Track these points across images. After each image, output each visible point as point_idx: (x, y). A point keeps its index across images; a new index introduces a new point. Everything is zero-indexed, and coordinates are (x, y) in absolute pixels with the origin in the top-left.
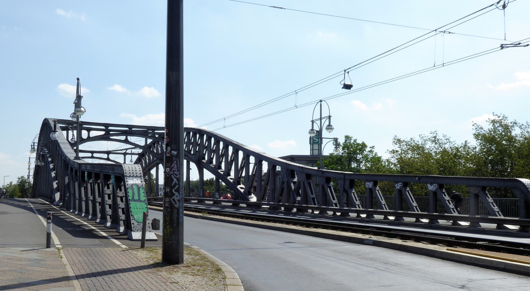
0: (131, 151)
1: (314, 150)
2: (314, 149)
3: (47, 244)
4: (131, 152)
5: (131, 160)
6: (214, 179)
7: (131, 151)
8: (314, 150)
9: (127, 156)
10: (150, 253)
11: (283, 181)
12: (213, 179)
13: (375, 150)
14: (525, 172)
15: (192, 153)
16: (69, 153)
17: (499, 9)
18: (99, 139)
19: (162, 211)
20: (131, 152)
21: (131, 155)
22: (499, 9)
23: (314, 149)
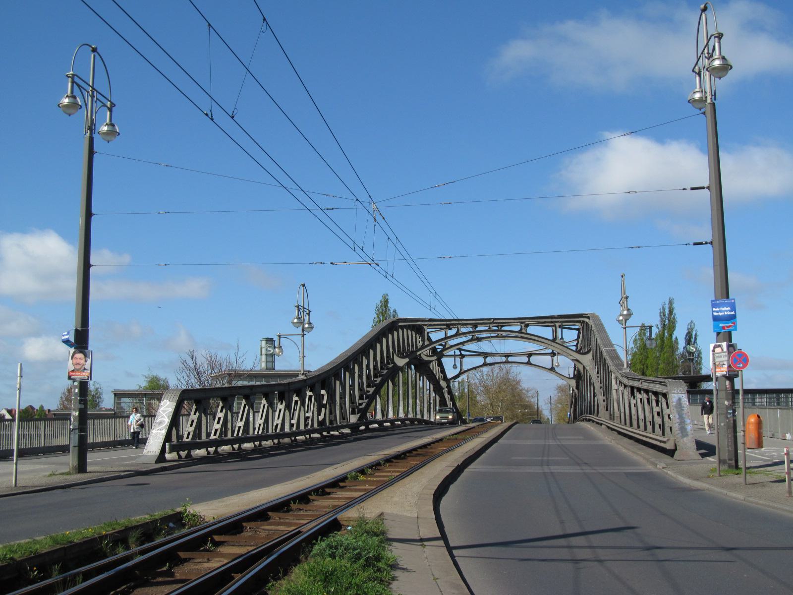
0: (455, 352)
5: (455, 365)
7: (455, 352)
9: (465, 360)
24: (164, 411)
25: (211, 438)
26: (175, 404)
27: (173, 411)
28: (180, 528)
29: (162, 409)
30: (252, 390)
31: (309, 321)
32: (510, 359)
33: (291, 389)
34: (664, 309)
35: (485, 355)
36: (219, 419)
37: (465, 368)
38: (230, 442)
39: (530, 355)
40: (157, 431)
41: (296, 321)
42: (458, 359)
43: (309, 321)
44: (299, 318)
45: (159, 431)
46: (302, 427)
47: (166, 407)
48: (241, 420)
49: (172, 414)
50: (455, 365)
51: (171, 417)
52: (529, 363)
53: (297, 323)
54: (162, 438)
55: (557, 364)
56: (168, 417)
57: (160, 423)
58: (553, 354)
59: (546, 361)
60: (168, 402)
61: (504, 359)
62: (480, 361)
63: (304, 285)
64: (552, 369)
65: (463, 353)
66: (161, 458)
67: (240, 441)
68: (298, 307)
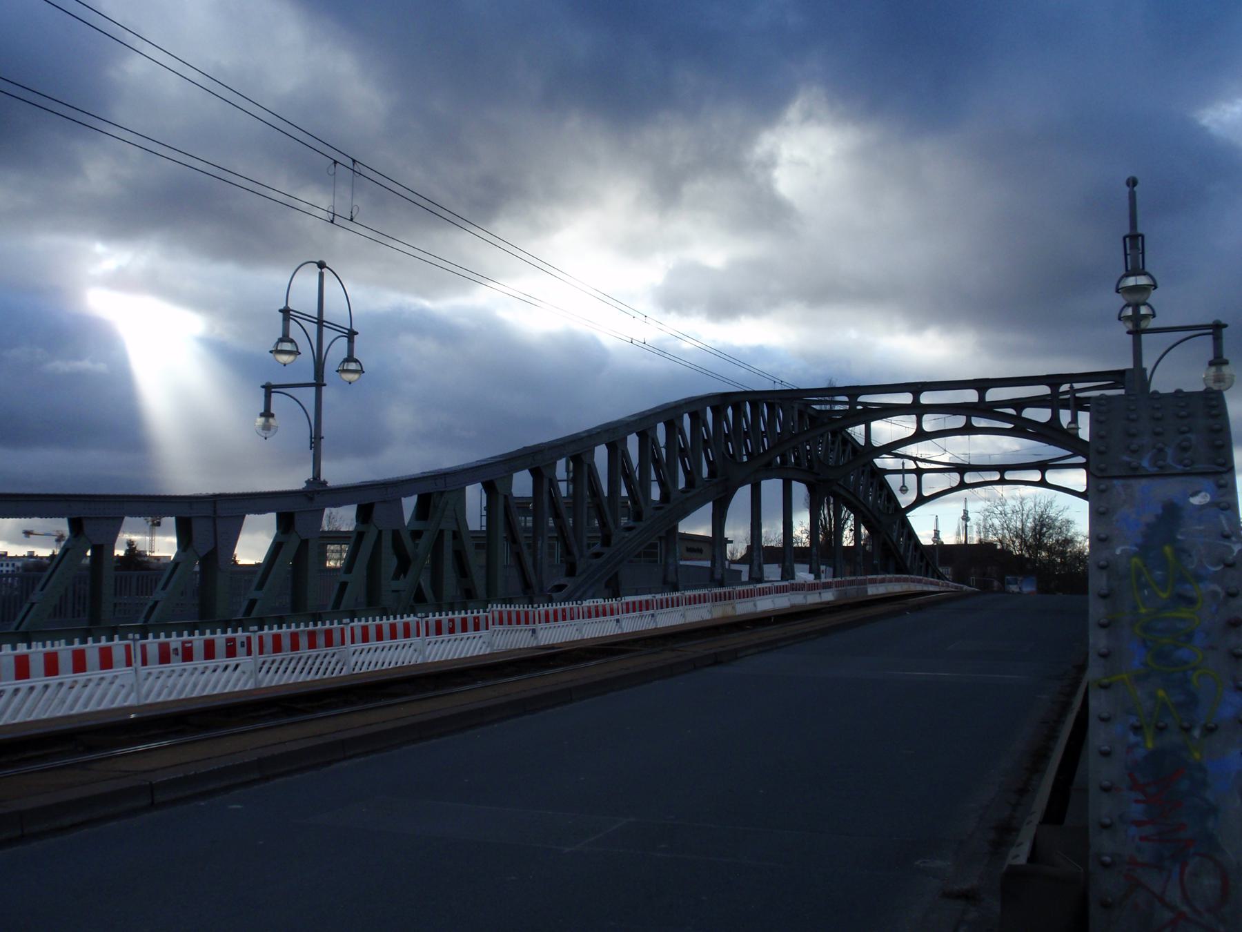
1: (903, 477)
2: (313, 389)
3: (281, 547)
4: (903, 467)
5: (904, 486)
6: (172, 558)
8: (903, 477)
9: (925, 476)
10: (156, 561)
11: (441, 527)
12: (170, 557)
13: (145, 522)
14: (1189, 435)
15: (745, 459)
16: (852, 473)
17: (458, 524)
18: (148, 569)
19: (759, 485)
20: (903, 467)
21: (901, 475)
22: (458, 524)
23: (313, 389)
35: (961, 469)
37: (926, 493)
39: (1043, 466)
42: (913, 477)
52: (1043, 483)
62: (955, 478)
65: (922, 465)
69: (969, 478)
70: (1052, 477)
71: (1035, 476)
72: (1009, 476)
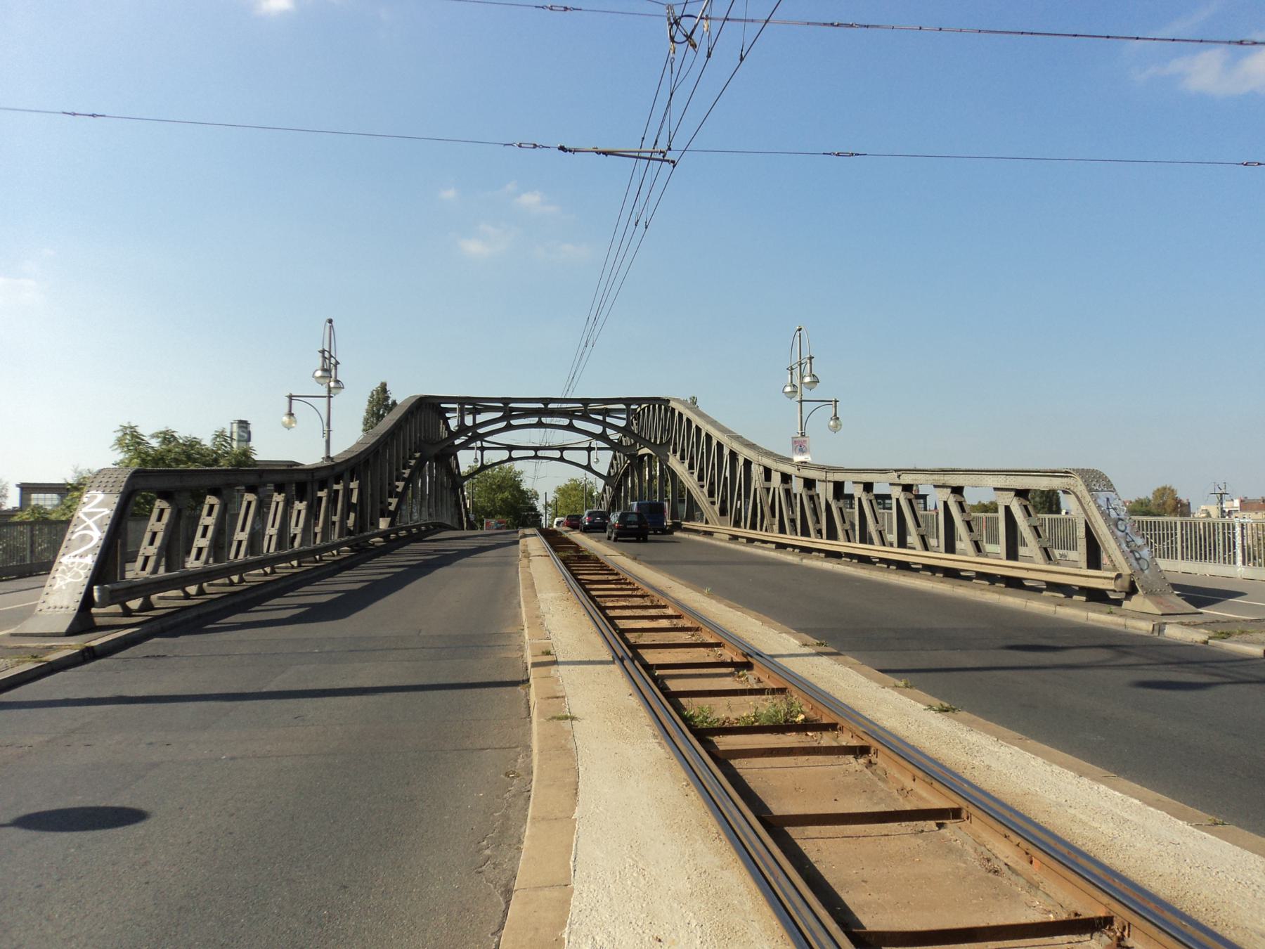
5: (476, 458)
9: (486, 452)
24: (90, 515)
25: (188, 565)
26: (117, 500)
27: (112, 515)
28: (1147, 501)
29: (86, 509)
30: (260, 476)
31: (792, 382)
32: (532, 453)
33: (315, 478)
34: (143, 436)
35: (510, 448)
36: (206, 528)
38: (260, 564)
39: (562, 449)
40: (72, 560)
41: (319, 373)
42: (479, 452)
43: (792, 382)
44: (324, 370)
45: (77, 560)
46: (269, 546)
47: (93, 507)
48: (243, 530)
49: (109, 522)
50: (476, 458)
51: (106, 528)
52: (561, 459)
53: (321, 377)
54: (83, 576)
55: (595, 460)
56: (100, 527)
57: (84, 539)
58: (589, 449)
59: (581, 457)
60: (100, 496)
61: (567, 455)
62: (504, 455)
63: (330, 321)
64: (588, 468)
65: (485, 445)
66: (83, 621)
67: (243, 568)
68: (323, 352)
69: (515, 454)
70: (567, 455)
71: (557, 454)
72: (540, 453)
